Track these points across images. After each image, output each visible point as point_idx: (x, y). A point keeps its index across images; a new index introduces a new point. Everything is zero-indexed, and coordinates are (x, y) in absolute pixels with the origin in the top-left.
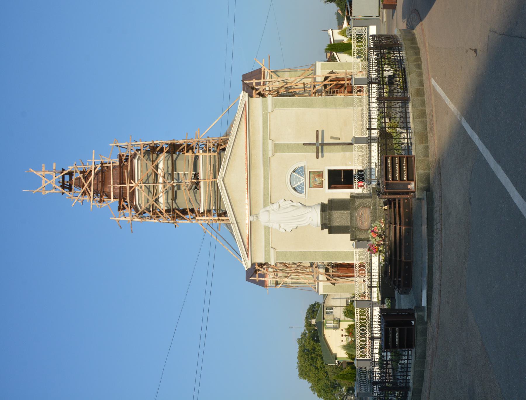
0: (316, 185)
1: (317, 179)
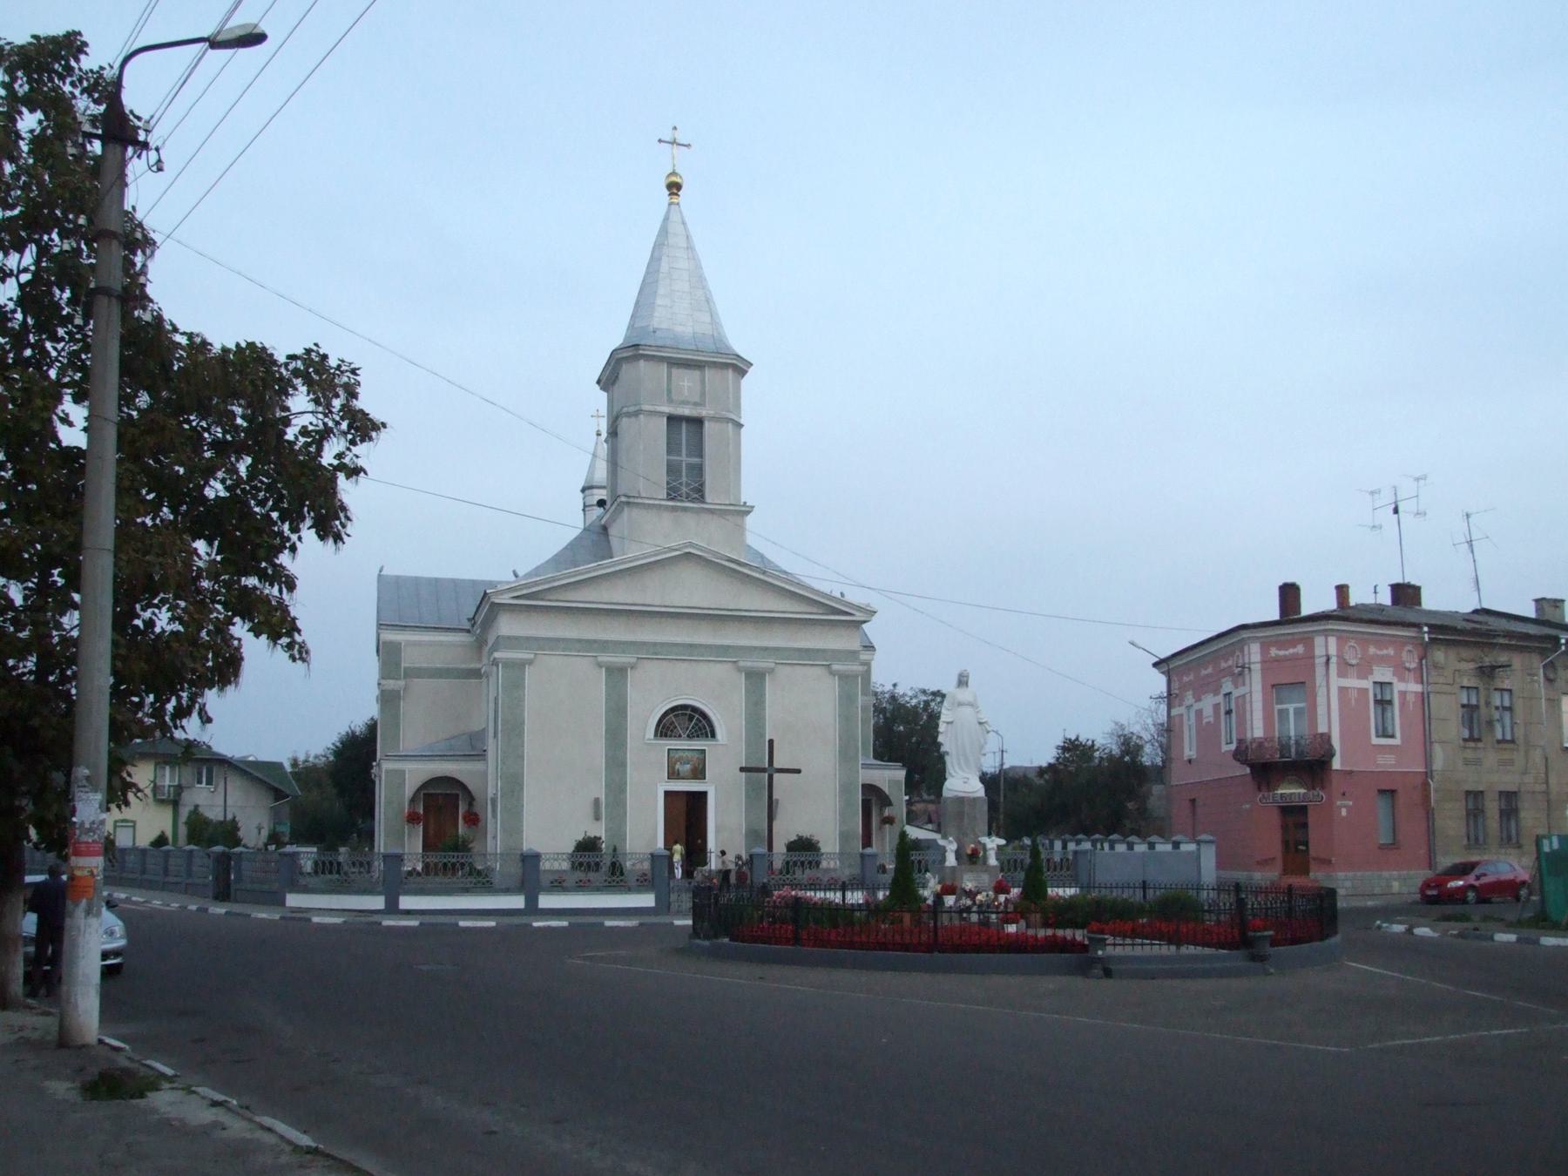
0: (675, 764)
1: (688, 767)
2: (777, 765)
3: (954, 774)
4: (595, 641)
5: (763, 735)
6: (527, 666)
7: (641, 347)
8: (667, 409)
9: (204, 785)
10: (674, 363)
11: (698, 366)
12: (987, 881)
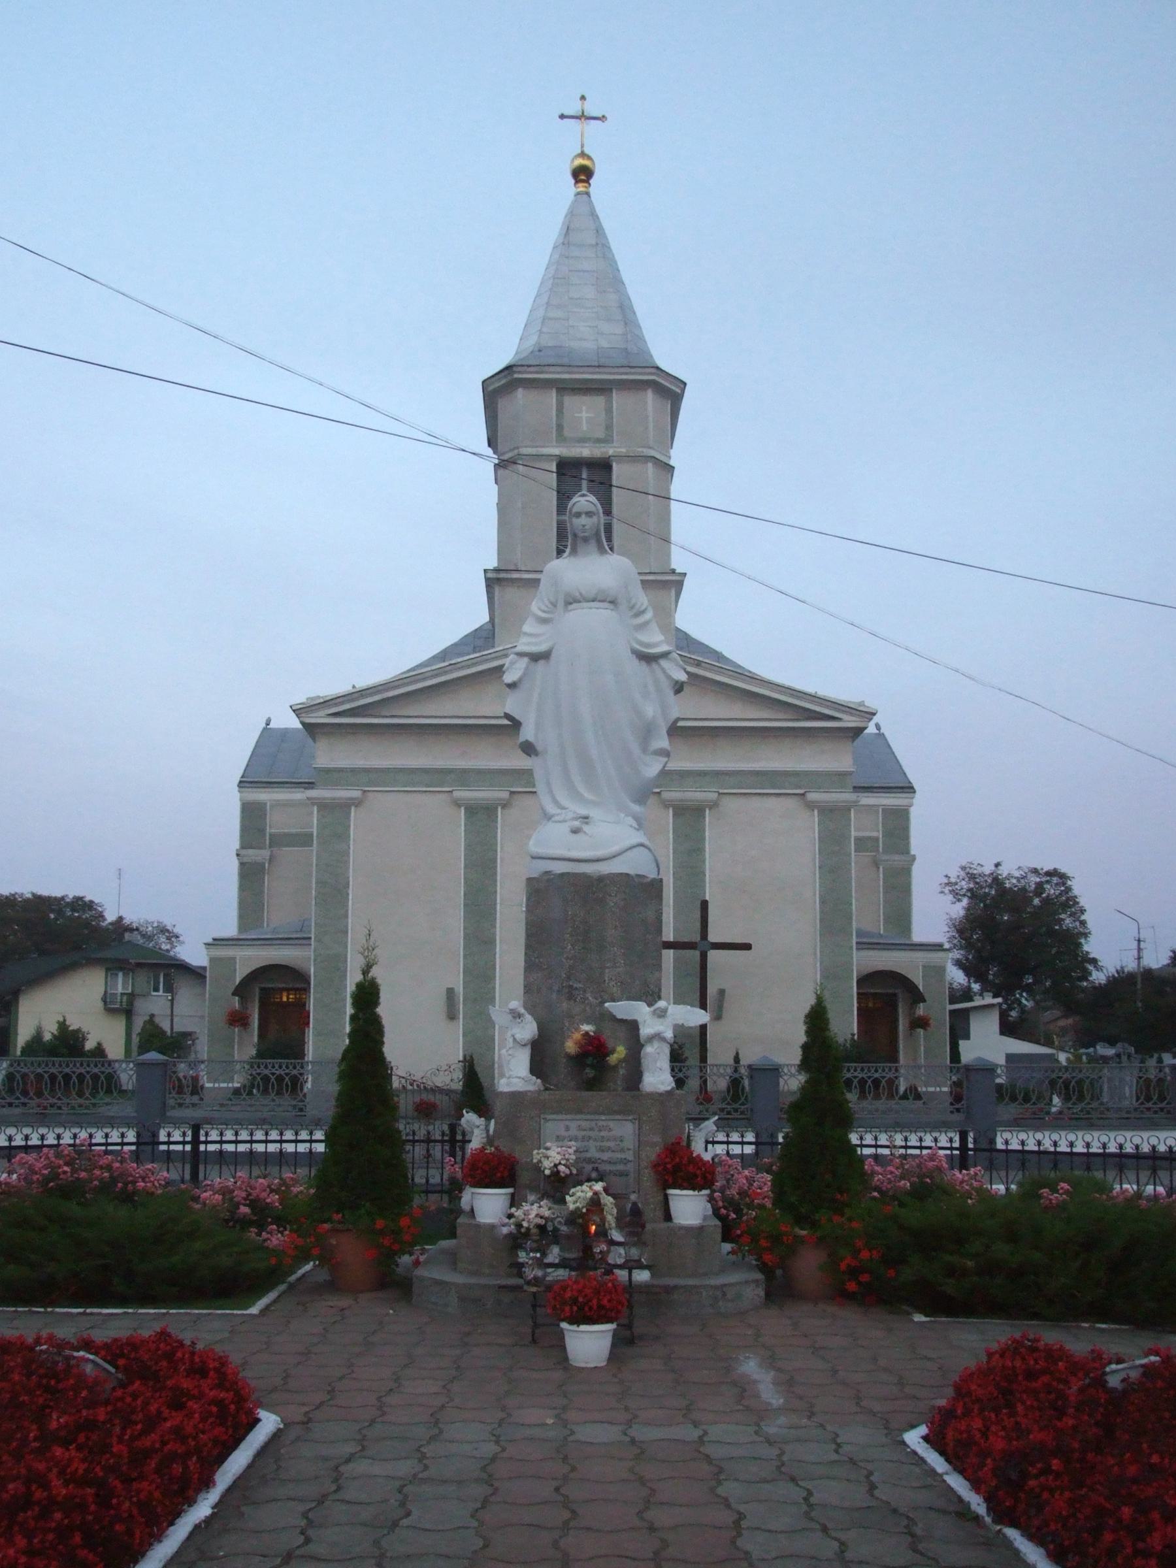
2: (713, 937)
3: (551, 809)
4: (450, 771)
6: (353, 809)
7: (515, 369)
8: (556, 451)
9: (161, 993)
10: (565, 388)
11: (601, 388)
12: (630, 1142)
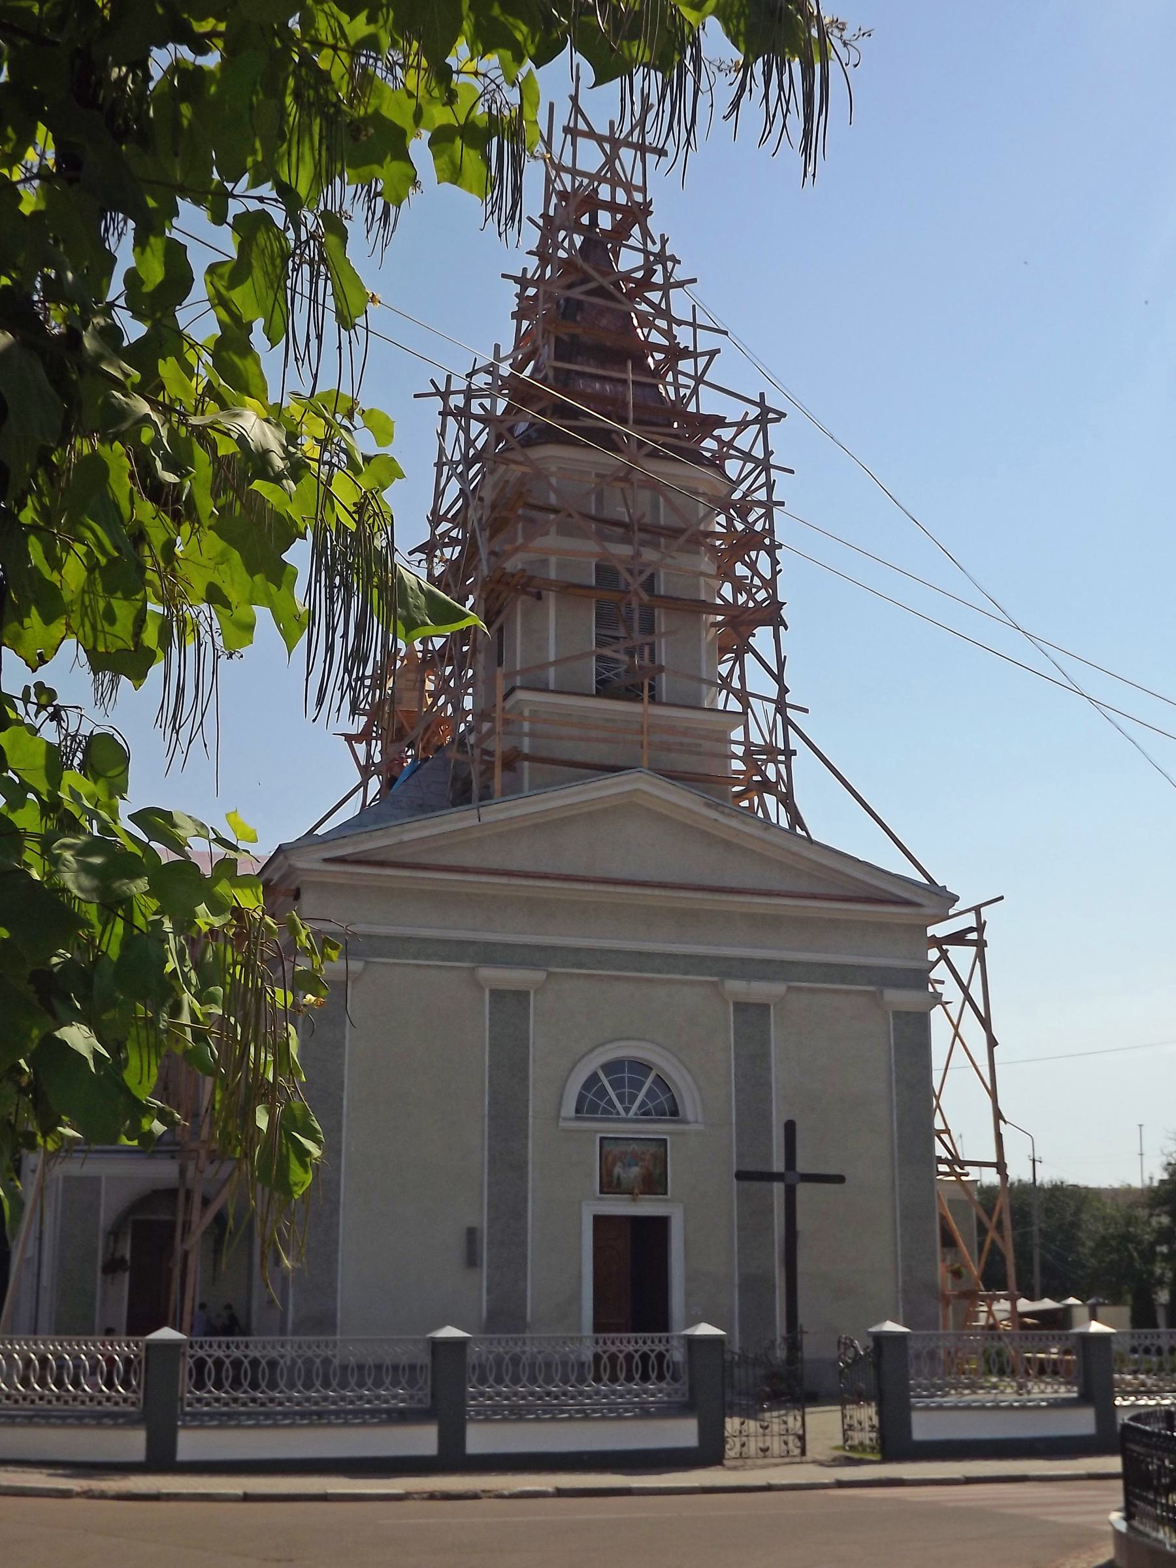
0: (614, 1164)
1: (636, 1170)
2: (803, 1165)
5: (766, 1116)
